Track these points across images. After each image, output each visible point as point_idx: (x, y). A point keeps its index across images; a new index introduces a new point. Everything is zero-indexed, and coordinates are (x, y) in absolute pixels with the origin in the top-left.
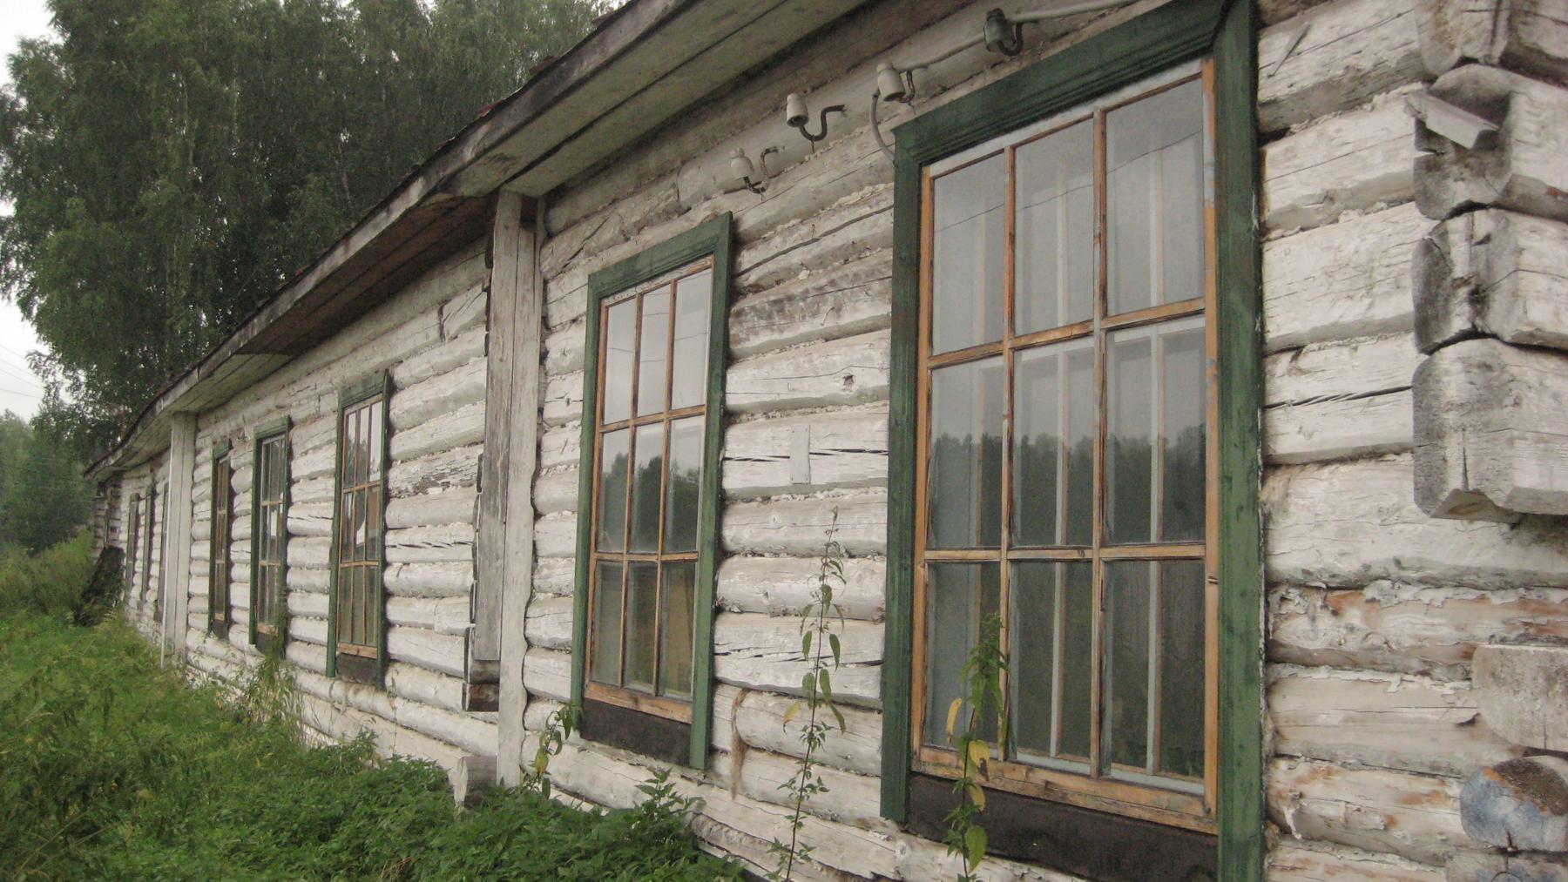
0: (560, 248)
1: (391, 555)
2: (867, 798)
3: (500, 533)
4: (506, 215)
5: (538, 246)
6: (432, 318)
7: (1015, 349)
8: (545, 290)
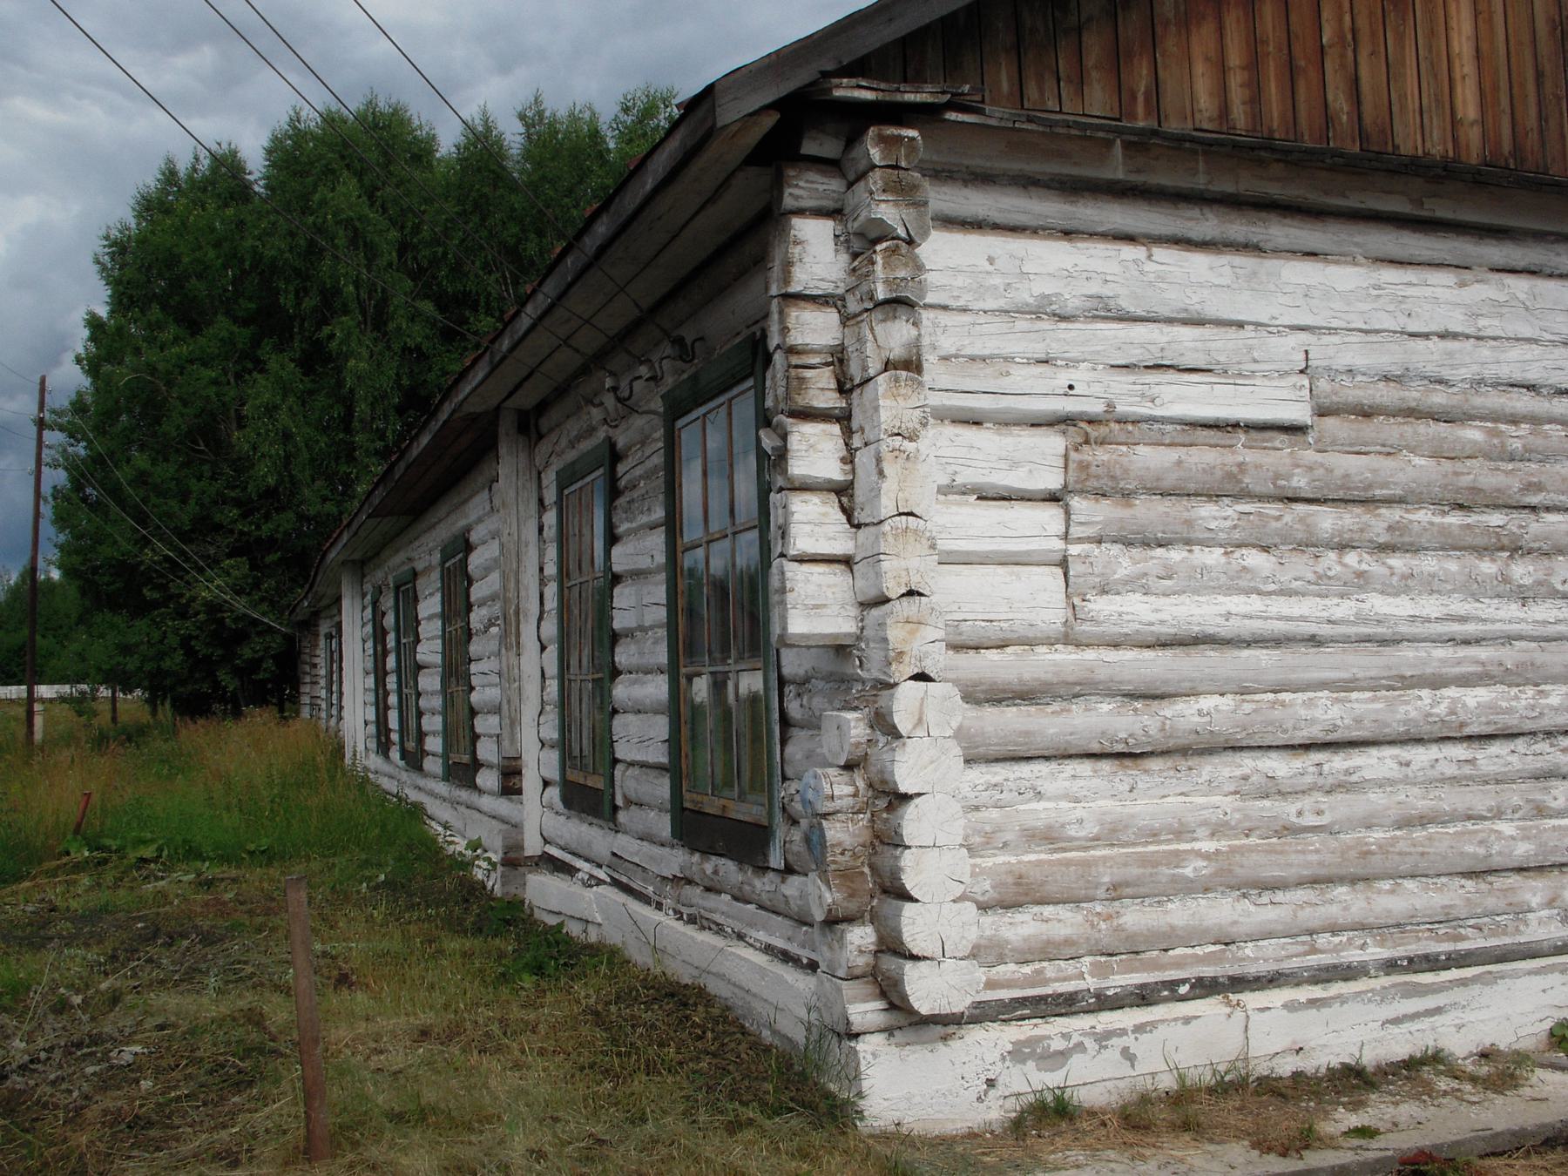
0: (544, 448)
1: (475, 681)
2: (663, 825)
3: (516, 663)
4: (506, 425)
5: (532, 445)
6: (486, 493)
7: (708, 542)
8: (539, 478)
